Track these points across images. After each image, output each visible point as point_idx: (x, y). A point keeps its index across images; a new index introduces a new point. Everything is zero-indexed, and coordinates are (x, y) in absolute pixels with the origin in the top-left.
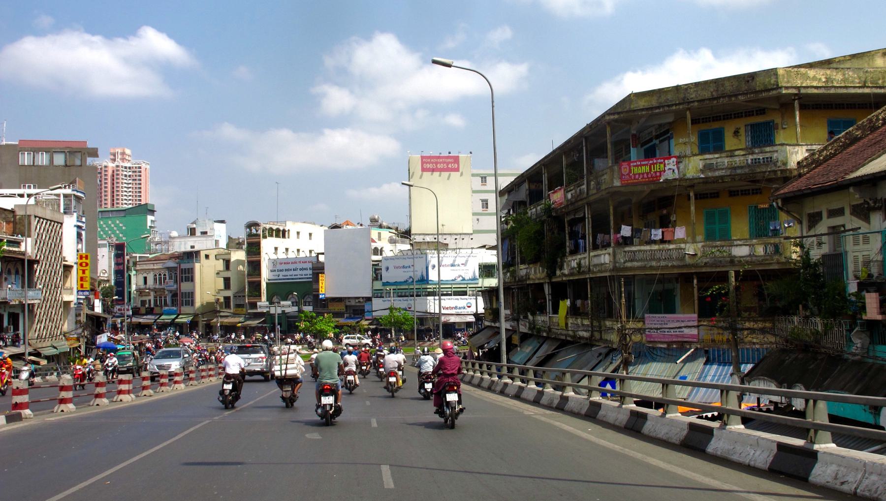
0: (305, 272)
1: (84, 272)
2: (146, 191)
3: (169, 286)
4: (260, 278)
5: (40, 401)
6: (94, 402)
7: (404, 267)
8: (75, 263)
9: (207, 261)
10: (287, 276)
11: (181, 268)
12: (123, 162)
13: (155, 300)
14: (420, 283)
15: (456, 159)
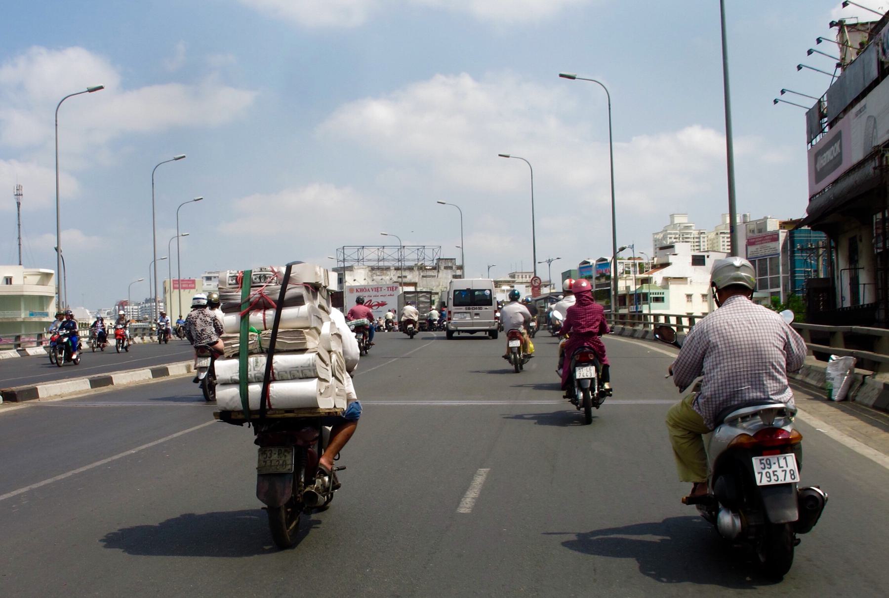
15: (193, 282)
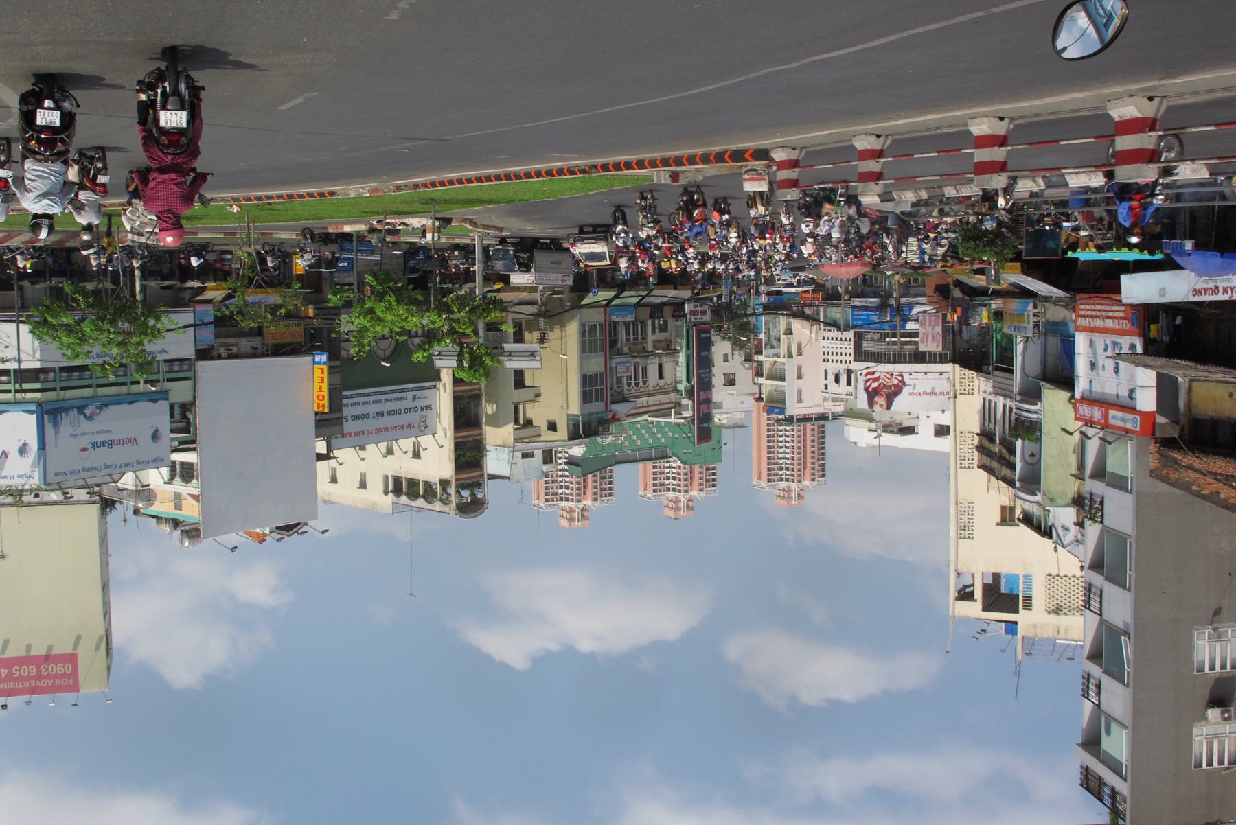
0: (358, 410)
4: (454, 392)
7: (110, 444)
9: (551, 418)
10: (397, 399)
11: (603, 403)
12: (571, 507)
13: (646, 334)
14: (61, 404)
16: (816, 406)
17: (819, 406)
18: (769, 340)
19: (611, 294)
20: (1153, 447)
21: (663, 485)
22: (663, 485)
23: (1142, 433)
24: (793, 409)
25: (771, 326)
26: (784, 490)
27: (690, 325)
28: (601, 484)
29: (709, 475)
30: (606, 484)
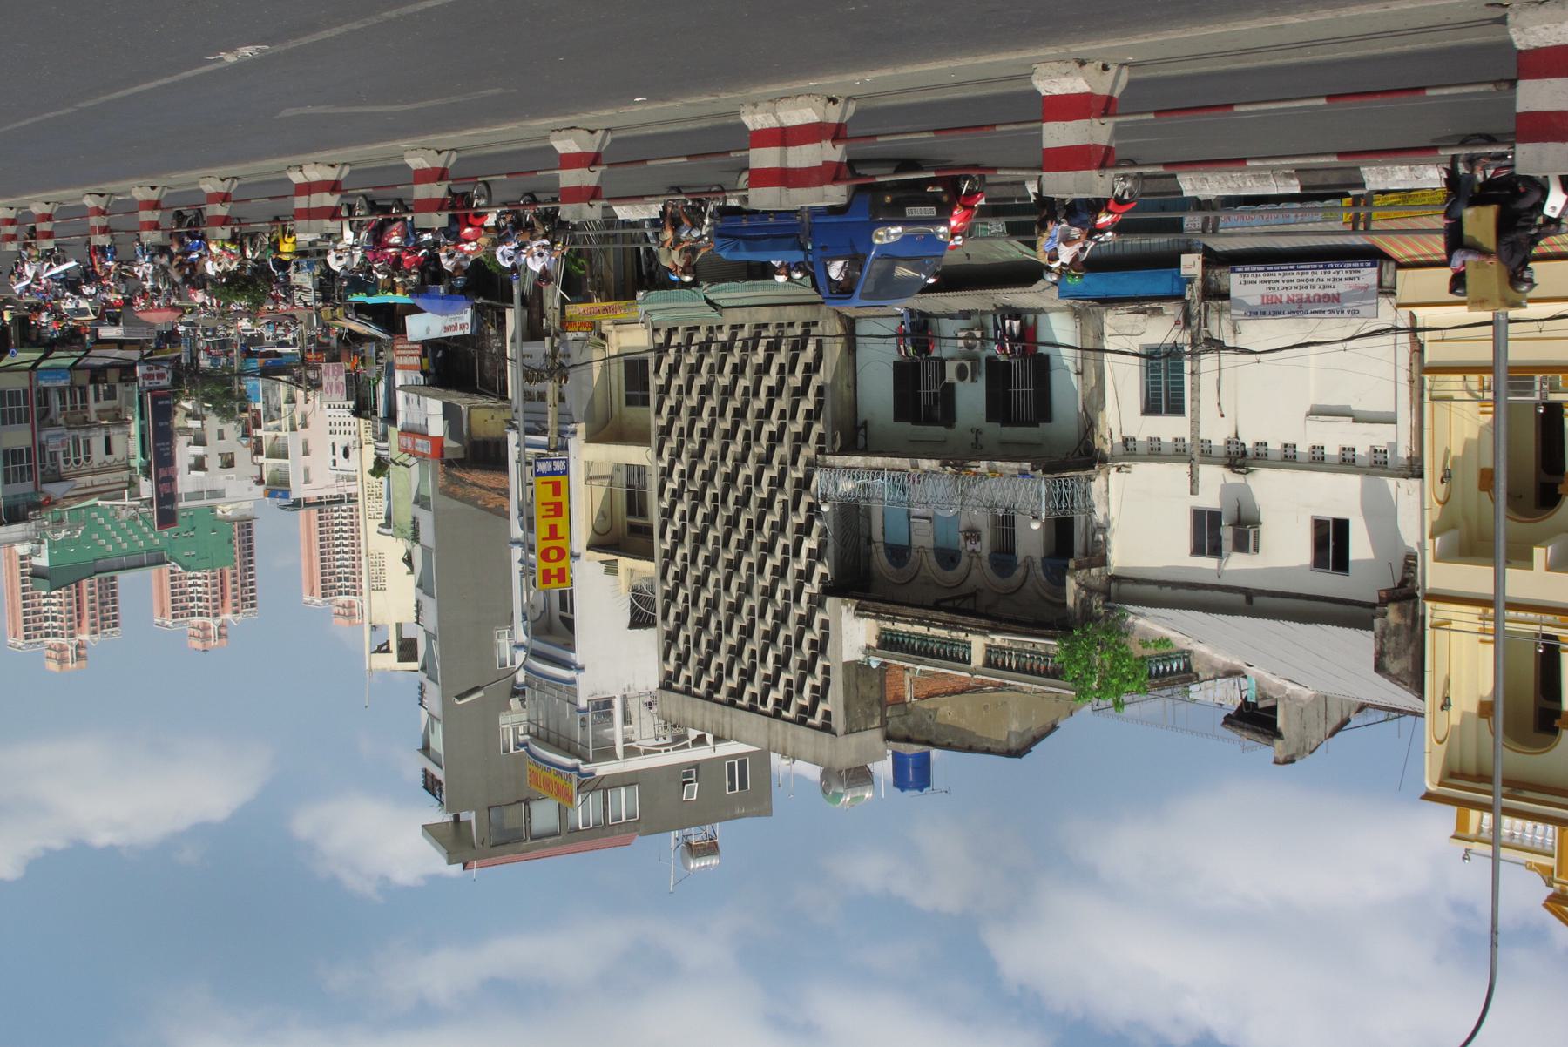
1: (553, 529)
2: (12, 592)
3: (58, 435)
5: (936, 131)
6: (162, 192)
8: (578, 556)
12: (61, 645)
13: (87, 402)
16: (327, 487)
17: (332, 487)
18: (268, 411)
19: (37, 355)
20: (440, 468)
21: (186, 608)
22: (186, 608)
23: (433, 456)
24: (298, 491)
25: (270, 393)
26: (344, 606)
27: (144, 390)
28: (102, 612)
29: (246, 593)
30: (108, 611)
